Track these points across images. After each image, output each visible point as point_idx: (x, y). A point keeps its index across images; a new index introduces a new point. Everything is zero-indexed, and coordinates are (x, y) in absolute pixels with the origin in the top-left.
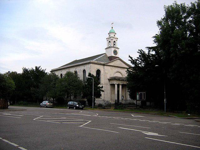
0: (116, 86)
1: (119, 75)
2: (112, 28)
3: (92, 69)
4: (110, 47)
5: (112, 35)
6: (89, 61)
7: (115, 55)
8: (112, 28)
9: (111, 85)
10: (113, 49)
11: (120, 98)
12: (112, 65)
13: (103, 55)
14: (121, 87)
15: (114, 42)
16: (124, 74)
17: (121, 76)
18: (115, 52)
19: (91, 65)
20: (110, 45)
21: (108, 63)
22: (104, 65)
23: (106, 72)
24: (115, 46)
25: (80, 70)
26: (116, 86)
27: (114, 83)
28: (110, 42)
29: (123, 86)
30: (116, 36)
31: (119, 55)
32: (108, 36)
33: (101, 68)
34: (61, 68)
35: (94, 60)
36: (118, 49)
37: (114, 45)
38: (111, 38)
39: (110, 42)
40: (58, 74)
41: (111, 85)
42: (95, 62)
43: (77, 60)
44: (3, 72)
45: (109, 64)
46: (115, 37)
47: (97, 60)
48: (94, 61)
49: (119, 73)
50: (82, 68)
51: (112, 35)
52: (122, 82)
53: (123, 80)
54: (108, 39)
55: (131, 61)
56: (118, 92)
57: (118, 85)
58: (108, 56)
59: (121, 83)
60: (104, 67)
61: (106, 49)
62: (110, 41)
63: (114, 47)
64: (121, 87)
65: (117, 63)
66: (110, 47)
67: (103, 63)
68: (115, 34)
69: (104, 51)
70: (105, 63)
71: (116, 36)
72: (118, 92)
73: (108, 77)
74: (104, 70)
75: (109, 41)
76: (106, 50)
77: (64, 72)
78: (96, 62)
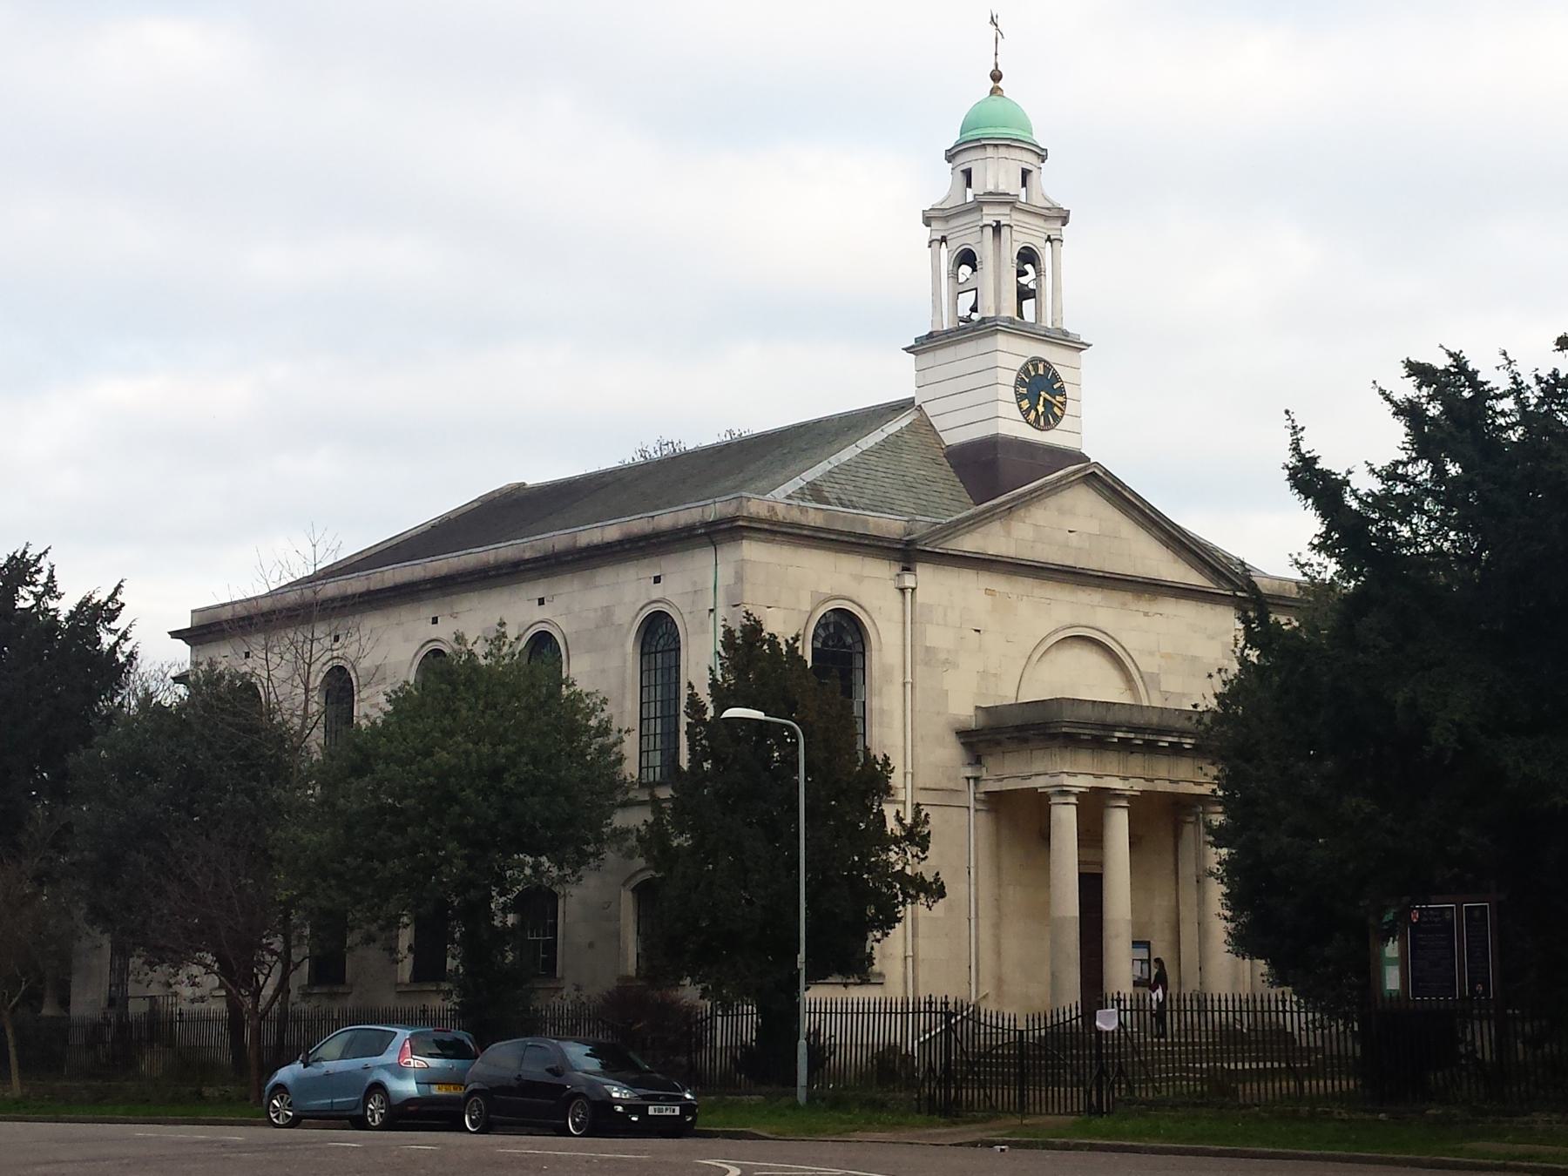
0: (1065, 819)
1: (1088, 681)
2: (996, 76)
3: (787, 593)
4: (973, 329)
5: (997, 173)
6: (557, 539)
7: (1035, 424)
8: (996, 76)
9: (997, 803)
10: (1012, 354)
11: (1121, 971)
12: (1126, 528)
13: (893, 427)
14: (1119, 824)
15: (1028, 256)
16: (1188, 658)
17: (1126, 699)
18: (1041, 390)
19: (752, 551)
20: (967, 300)
21: (955, 528)
22: (906, 554)
23: (937, 637)
24: (1028, 305)
25: (593, 631)
26: (1065, 819)
27: (1038, 783)
28: (967, 258)
29: (1160, 819)
30: (1051, 185)
31: (1096, 426)
32: (940, 186)
33: (869, 587)
34: (331, 589)
35: (780, 493)
36: (1079, 346)
37: (1024, 294)
38: (990, 215)
39: (967, 258)
40: (283, 676)
41: (997, 803)
42: (795, 515)
43: (531, 481)
44: (181, 507)
45: (969, 543)
46: (1038, 201)
47: (814, 492)
48: (778, 497)
49: (1091, 660)
50: (627, 593)
51: (997, 173)
52: (1137, 764)
53: (1150, 748)
54: (939, 229)
55: (714, 680)
56: (1092, 886)
57: (1093, 806)
58: (952, 438)
59: (1120, 776)
60: (909, 581)
61: (925, 345)
62: (970, 241)
63: (1017, 328)
64: (1119, 824)
65: (1067, 526)
66: (973, 329)
67: (890, 525)
68: (1029, 160)
69: (889, 377)
70: (923, 524)
71: (1051, 185)
72: (1092, 886)
73: (963, 707)
74: (912, 622)
75: (956, 245)
76: (928, 359)
77: (388, 653)
78: (814, 516)
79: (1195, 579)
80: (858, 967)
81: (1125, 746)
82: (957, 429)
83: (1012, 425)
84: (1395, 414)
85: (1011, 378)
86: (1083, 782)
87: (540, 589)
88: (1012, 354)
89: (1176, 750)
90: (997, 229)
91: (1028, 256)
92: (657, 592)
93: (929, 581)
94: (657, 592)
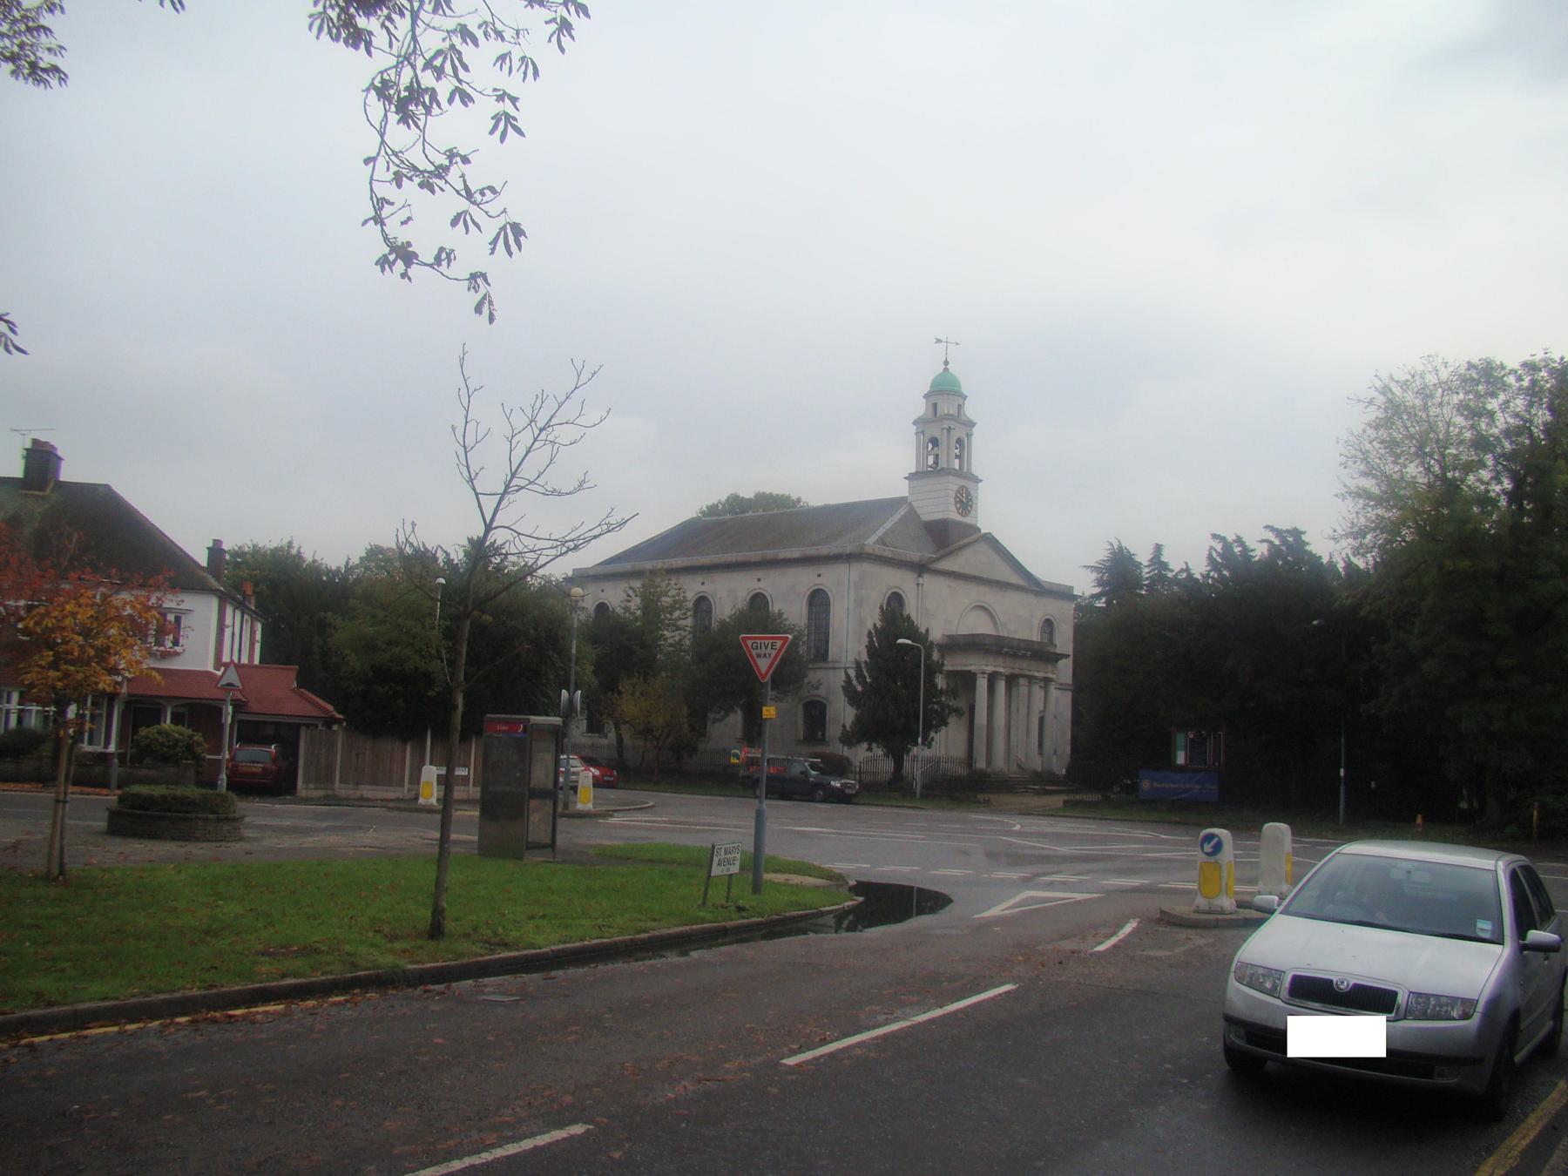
5: (946, 407)
8: (946, 363)
18: (965, 502)
19: (866, 567)
22: (921, 568)
26: (982, 684)
27: (973, 668)
31: (991, 515)
49: (982, 616)
50: (806, 580)
53: (1015, 655)
57: (992, 678)
58: (925, 518)
62: (937, 434)
75: (928, 435)
79: (1022, 582)
80: (928, 743)
81: (1007, 654)
82: (929, 513)
83: (953, 515)
84: (973, 424)
85: (952, 494)
86: (990, 669)
87: (759, 574)
88: (954, 484)
89: (1024, 656)
90: (949, 429)
91: (959, 441)
92: (819, 580)
93: (928, 581)
94: (819, 580)
